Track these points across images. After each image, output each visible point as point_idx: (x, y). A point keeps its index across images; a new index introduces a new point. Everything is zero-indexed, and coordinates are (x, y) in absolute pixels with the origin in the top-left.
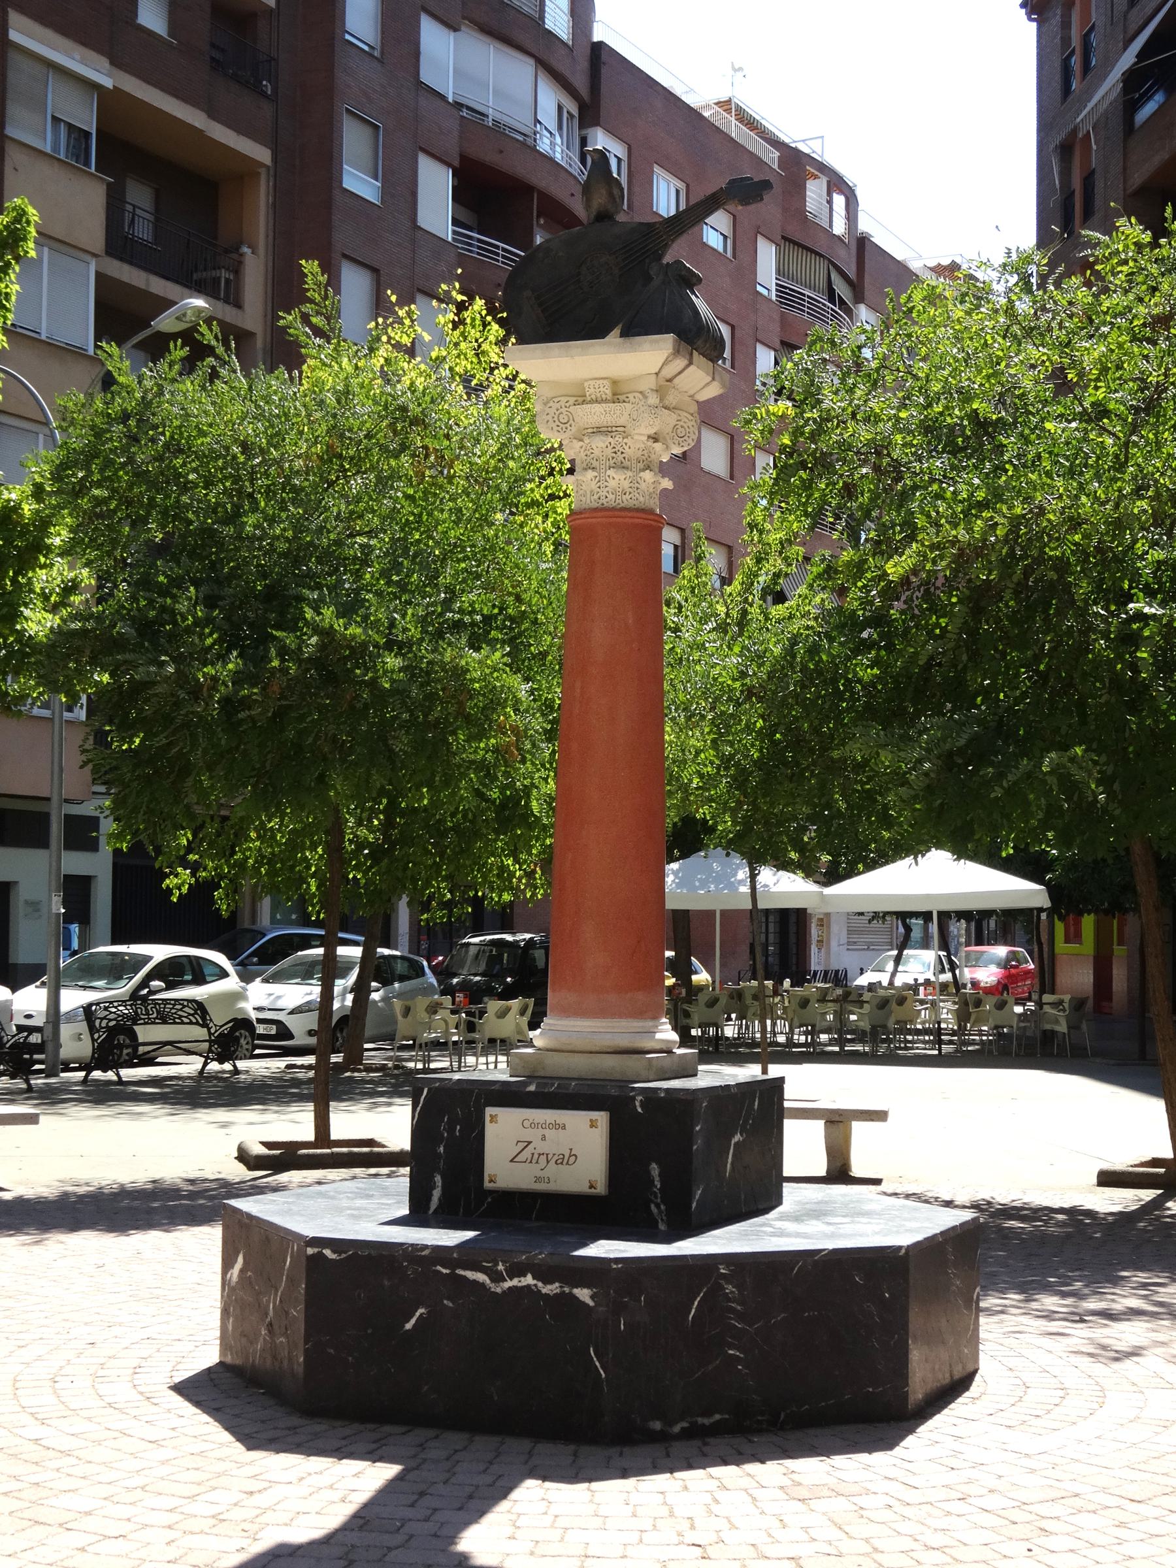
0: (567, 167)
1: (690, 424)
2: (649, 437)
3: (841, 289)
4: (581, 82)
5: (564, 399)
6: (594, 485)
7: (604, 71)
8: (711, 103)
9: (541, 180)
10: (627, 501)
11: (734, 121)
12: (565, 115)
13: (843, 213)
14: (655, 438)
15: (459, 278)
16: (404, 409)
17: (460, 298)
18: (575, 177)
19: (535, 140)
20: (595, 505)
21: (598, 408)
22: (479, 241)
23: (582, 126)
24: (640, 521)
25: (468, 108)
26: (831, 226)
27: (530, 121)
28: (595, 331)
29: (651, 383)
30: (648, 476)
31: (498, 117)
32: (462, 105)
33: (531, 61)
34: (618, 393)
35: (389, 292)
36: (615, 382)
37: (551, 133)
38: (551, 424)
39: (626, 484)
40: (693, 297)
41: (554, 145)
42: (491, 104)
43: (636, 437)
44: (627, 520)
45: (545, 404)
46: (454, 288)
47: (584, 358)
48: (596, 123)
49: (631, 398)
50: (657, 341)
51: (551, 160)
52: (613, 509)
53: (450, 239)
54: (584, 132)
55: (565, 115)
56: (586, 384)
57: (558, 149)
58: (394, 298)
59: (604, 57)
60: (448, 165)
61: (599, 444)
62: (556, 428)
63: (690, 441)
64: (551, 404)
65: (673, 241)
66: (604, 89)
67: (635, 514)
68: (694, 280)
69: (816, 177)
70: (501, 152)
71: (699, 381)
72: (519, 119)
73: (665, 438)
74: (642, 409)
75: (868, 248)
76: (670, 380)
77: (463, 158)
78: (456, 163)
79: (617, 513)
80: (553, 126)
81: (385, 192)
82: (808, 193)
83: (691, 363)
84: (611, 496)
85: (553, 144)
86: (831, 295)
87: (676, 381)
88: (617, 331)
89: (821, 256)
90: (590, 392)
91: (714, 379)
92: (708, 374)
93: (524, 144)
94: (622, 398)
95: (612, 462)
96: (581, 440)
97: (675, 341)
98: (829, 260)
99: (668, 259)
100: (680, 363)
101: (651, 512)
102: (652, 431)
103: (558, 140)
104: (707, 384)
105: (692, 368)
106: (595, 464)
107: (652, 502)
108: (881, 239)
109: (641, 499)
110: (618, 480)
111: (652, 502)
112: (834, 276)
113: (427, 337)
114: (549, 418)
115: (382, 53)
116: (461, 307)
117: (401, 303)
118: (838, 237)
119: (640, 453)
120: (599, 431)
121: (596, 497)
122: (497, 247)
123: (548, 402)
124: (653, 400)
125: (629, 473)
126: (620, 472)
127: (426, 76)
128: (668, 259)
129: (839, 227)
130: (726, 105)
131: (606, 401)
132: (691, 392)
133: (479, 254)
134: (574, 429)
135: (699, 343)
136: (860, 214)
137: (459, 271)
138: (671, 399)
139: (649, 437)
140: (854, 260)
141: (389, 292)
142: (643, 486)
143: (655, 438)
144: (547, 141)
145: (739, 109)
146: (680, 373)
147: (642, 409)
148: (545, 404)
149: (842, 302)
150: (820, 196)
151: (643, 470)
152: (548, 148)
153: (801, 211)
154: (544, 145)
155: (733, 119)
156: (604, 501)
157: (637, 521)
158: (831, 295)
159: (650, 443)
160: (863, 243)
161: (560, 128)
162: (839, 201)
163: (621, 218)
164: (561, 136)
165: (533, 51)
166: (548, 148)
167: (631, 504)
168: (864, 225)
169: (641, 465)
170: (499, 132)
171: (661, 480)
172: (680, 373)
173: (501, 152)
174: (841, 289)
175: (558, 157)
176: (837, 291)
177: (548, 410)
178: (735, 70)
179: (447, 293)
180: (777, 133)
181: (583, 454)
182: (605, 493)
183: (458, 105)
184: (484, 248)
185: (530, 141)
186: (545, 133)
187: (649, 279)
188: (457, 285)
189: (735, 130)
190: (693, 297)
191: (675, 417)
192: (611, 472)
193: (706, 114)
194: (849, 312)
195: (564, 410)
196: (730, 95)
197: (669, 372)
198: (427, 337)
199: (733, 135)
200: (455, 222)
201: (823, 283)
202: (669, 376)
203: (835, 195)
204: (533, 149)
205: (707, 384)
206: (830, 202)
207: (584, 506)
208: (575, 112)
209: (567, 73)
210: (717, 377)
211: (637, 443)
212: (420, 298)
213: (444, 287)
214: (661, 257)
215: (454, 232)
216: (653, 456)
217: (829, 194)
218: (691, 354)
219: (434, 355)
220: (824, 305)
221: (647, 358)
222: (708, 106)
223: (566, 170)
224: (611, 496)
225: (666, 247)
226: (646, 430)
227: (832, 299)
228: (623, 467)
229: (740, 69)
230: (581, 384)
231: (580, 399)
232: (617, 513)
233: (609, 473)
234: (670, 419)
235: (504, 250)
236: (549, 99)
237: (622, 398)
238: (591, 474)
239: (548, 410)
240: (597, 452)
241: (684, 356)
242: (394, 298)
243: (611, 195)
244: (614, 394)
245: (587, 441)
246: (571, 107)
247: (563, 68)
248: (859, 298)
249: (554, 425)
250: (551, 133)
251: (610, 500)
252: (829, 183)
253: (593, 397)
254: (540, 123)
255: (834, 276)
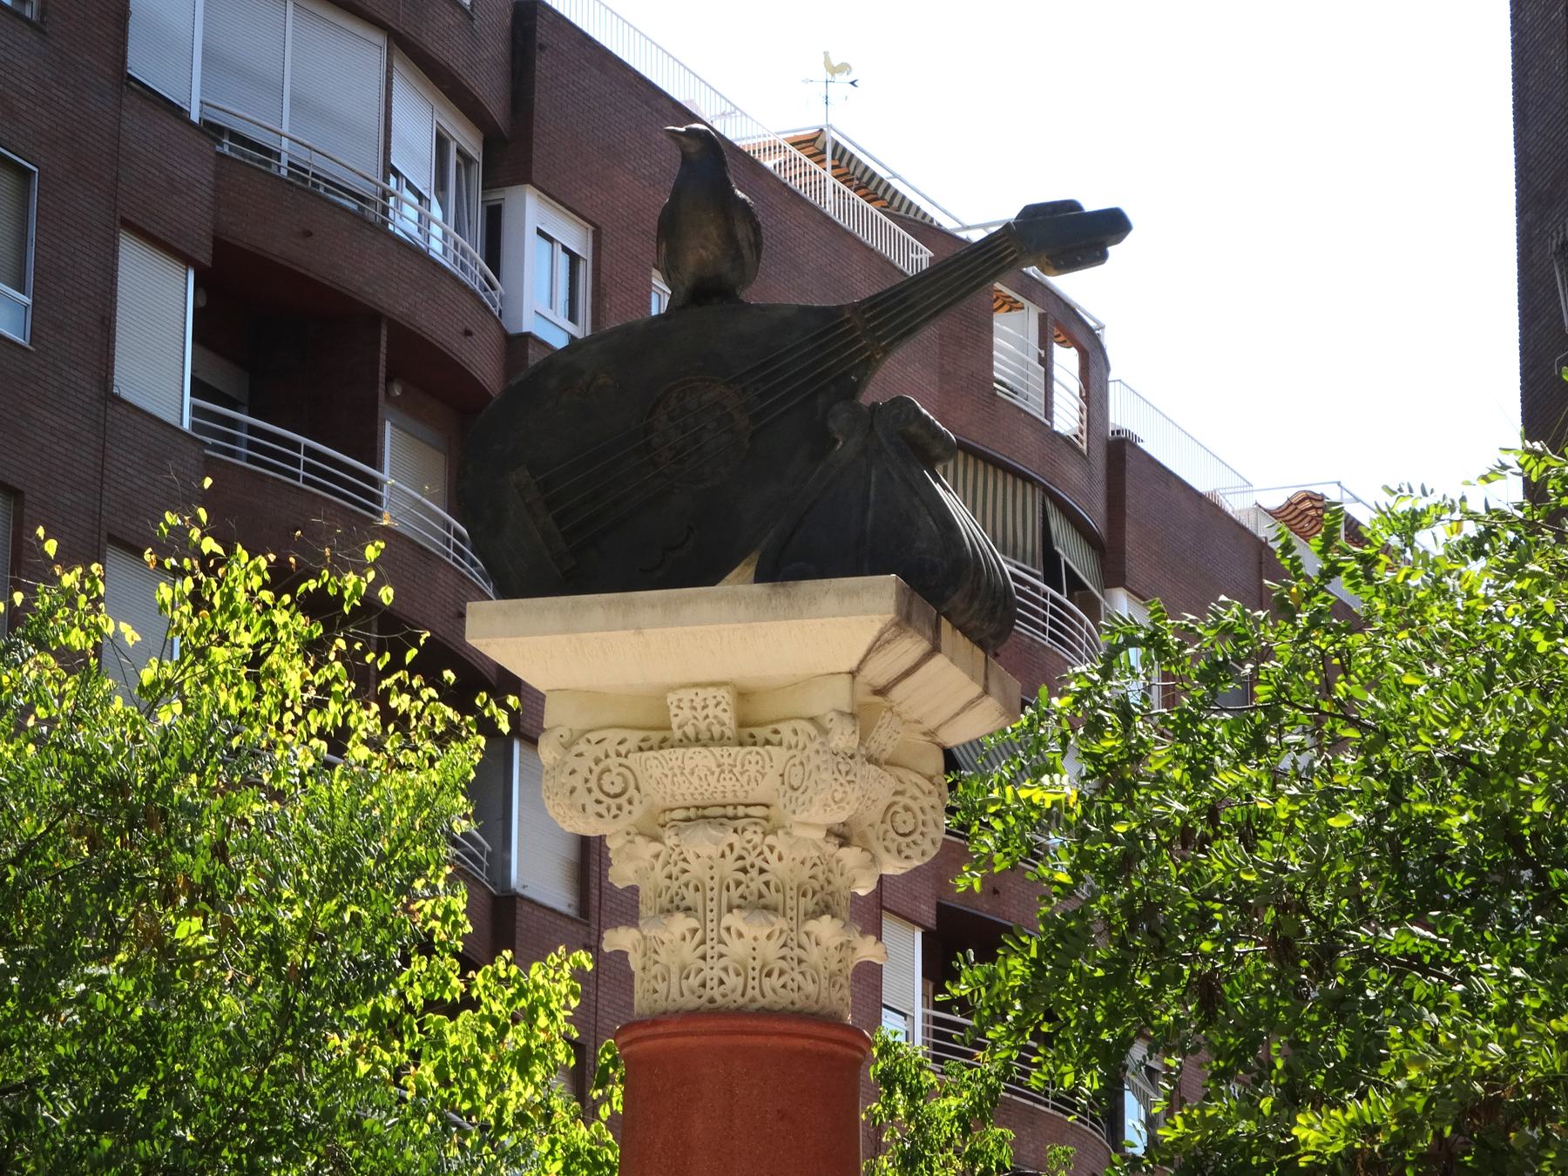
0: (456, 270)
1: (926, 802)
2: (830, 832)
3: (1073, 554)
4: (491, 89)
5: (614, 736)
6: (688, 952)
7: (542, 63)
8: (780, 140)
9: (397, 299)
10: (773, 992)
11: (831, 181)
12: (453, 158)
13: (1075, 385)
14: (842, 836)
15: (206, 499)
16: (118, 786)
17: (209, 545)
18: (474, 294)
19: (385, 210)
20: (691, 1002)
21: (700, 758)
22: (252, 430)
23: (490, 183)
24: (806, 1043)
25: (236, 137)
26: (1049, 413)
27: (374, 170)
28: (700, 570)
29: (839, 695)
30: (826, 929)
31: (303, 156)
32: (220, 130)
33: (379, 39)
34: (750, 720)
35: (41, 531)
36: (743, 695)
37: (420, 196)
38: (582, 797)
39: (771, 950)
40: (938, 487)
41: (424, 222)
42: (285, 129)
43: (798, 832)
44: (774, 1041)
45: (567, 747)
46: (196, 521)
47: (669, 631)
48: (522, 175)
49: (786, 730)
50: (854, 593)
51: (418, 254)
52: (739, 1012)
53: (186, 426)
54: (495, 196)
55: (453, 158)
56: (672, 698)
57: (436, 230)
58: (51, 547)
59: (543, 34)
60: (187, 260)
61: (704, 849)
62: (592, 808)
63: (927, 845)
64: (582, 746)
65: (886, 352)
66: (543, 102)
67: (793, 1026)
68: (938, 450)
69: (1013, 306)
70: (308, 234)
71: (950, 694)
72: (348, 161)
73: (863, 836)
74: (816, 760)
75: (1131, 462)
76: (881, 692)
77: (221, 246)
78: (205, 257)
79: (750, 1024)
80: (425, 182)
81: (40, 316)
82: (997, 340)
83: (936, 649)
84: (733, 981)
85: (424, 221)
86: (1051, 567)
87: (897, 693)
88: (746, 569)
89: (1026, 479)
90: (682, 717)
91: (986, 691)
92: (973, 678)
93: (359, 218)
94: (762, 733)
95: (735, 893)
96: (656, 839)
97: (900, 592)
98: (1048, 493)
99: (873, 394)
100: (910, 647)
101: (831, 1020)
102: (838, 817)
103: (436, 212)
104: (971, 704)
105: (939, 661)
106: (691, 897)
107: (835, 995)
108: (1157, 444)
109: (810, 988)
110: (750, 938)
111: (835, 995)
112: (1056, 524)
113: (130, 635)
114: (577, 781)
115: (43, 11)
116: (210, 565)
117: (67, 558)
118: (1066, 440)
119: (806, 872)
120: (702, 815)
121: (694, 981)
122: (295, 446)
123: (573, 743)
124: (843, 737)
125: (780, 923)
126: (759, 918)
127: (141, 65)
128: (873, 394)
129: (1067, 418)
130: (812, 145)
131: (721, 741)
132: (931, 724)
133: (250, 459)
134: (638, 810)
135: (957, 600)
136: (1114, 391)
137: (208, 482)
138: (885, 739)
139: (830, 832)
140: (1100, 489)
141: (41, 531)
142: (814, 955)
143: (842, 836)
144: (411, 213)
145: (840, 153)
146: (908, 673)
147: (816, 760)
148: (567, 747)
149: (1075, 585)
150: (1024, 347)
151: (815, 915)
152: (412, 229)
153: (982, 380)
154: (405, 220)
155: (828, 174)
156: (717, 993)
157: (806, 1043)
158: (1051, 567)
159: (831, 847)
160: (1120, 453)
161: (441, 185)
162: (1066, 360)
163: (751, 295)
164: (443, 205)
165: (385, 16)
166: (412, 229)
167: (783, 999)
168: (1122, 415)
169: (808, 903)
170: (305, 190)
171: (857, 940)
172: (908, 673)
173: (308, 234)
174: (1073, 554)
175: (436, 246)
176: (1064, 557)
177: (573, 763)
178: (834, 70)
179: (180, 533)
180: (926, 207)
181: (659, 874)
182: (717, 973)
183: (212, 130)
184: (263, 445)
185: (373, 213)
186: (408, 195)
187: (825, 442)
188: (203, 514)
189: (831, 195)
190: (938, 487)
191: (891, 783)
192: (734, 920)
193: (769, 164)
194: (1092, 607)
195: (613, 762)
196: (821, 123)
197: (881, 669)
198: (130, 635)
199: (829, 210)
200: (198, 388)
201: (1032, 542)
202: (881, 681)
203: (1057, 349)
204: (381, 229)
205: (971, 704)
206: (1046, 361)
207: (662, 1005)
208: (475, 150)
209: (458, 65)
210: (994, 687)
211: (796, 849)
212: (112, 554)
213: (170, 518)
214: (854, 391)
215: (196, 411)
216: (838, 882)
217: (1044, 343)
218: (937, 629)
219: (147, 676)
220: (1035, 589)
221: (831, 632)
222: (775, 148)
223: (455, 278)
224: (733, 981)
225: (868, 365)
226: (838, 816)
227: (1052, 578)
228: (761, 906)
229: (845, 68)
230: (658, 698)
231: (656, 736)
232: (750, 1024)
233: (728, 919)
234: (880, 786)
235: (310, 452)
236: (418, 123)
237: (762, 733)
238: (681, 924)
239: (573, 763)
240: (697, 869)
241: (920, 632)
242: (51, 547)
243: (730, 238)
244: (742, 724)
245: (670, 838)
246: (466, 139)
247: (451, 53)
248: (1113, 576)
249: (589, 801)
250: (420, 196)
251: (732, 991)
252: (1043, 319)
253: (690, 730)
254: (397, 173)
255: (1056, 524)
